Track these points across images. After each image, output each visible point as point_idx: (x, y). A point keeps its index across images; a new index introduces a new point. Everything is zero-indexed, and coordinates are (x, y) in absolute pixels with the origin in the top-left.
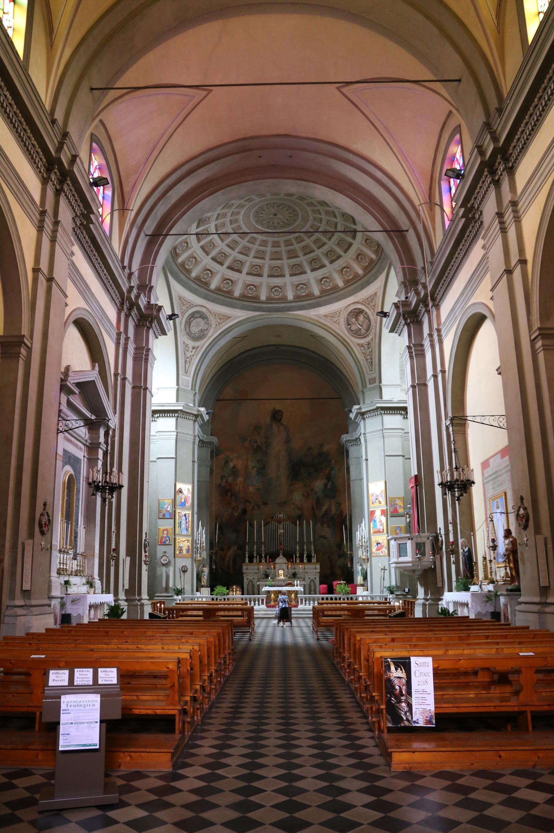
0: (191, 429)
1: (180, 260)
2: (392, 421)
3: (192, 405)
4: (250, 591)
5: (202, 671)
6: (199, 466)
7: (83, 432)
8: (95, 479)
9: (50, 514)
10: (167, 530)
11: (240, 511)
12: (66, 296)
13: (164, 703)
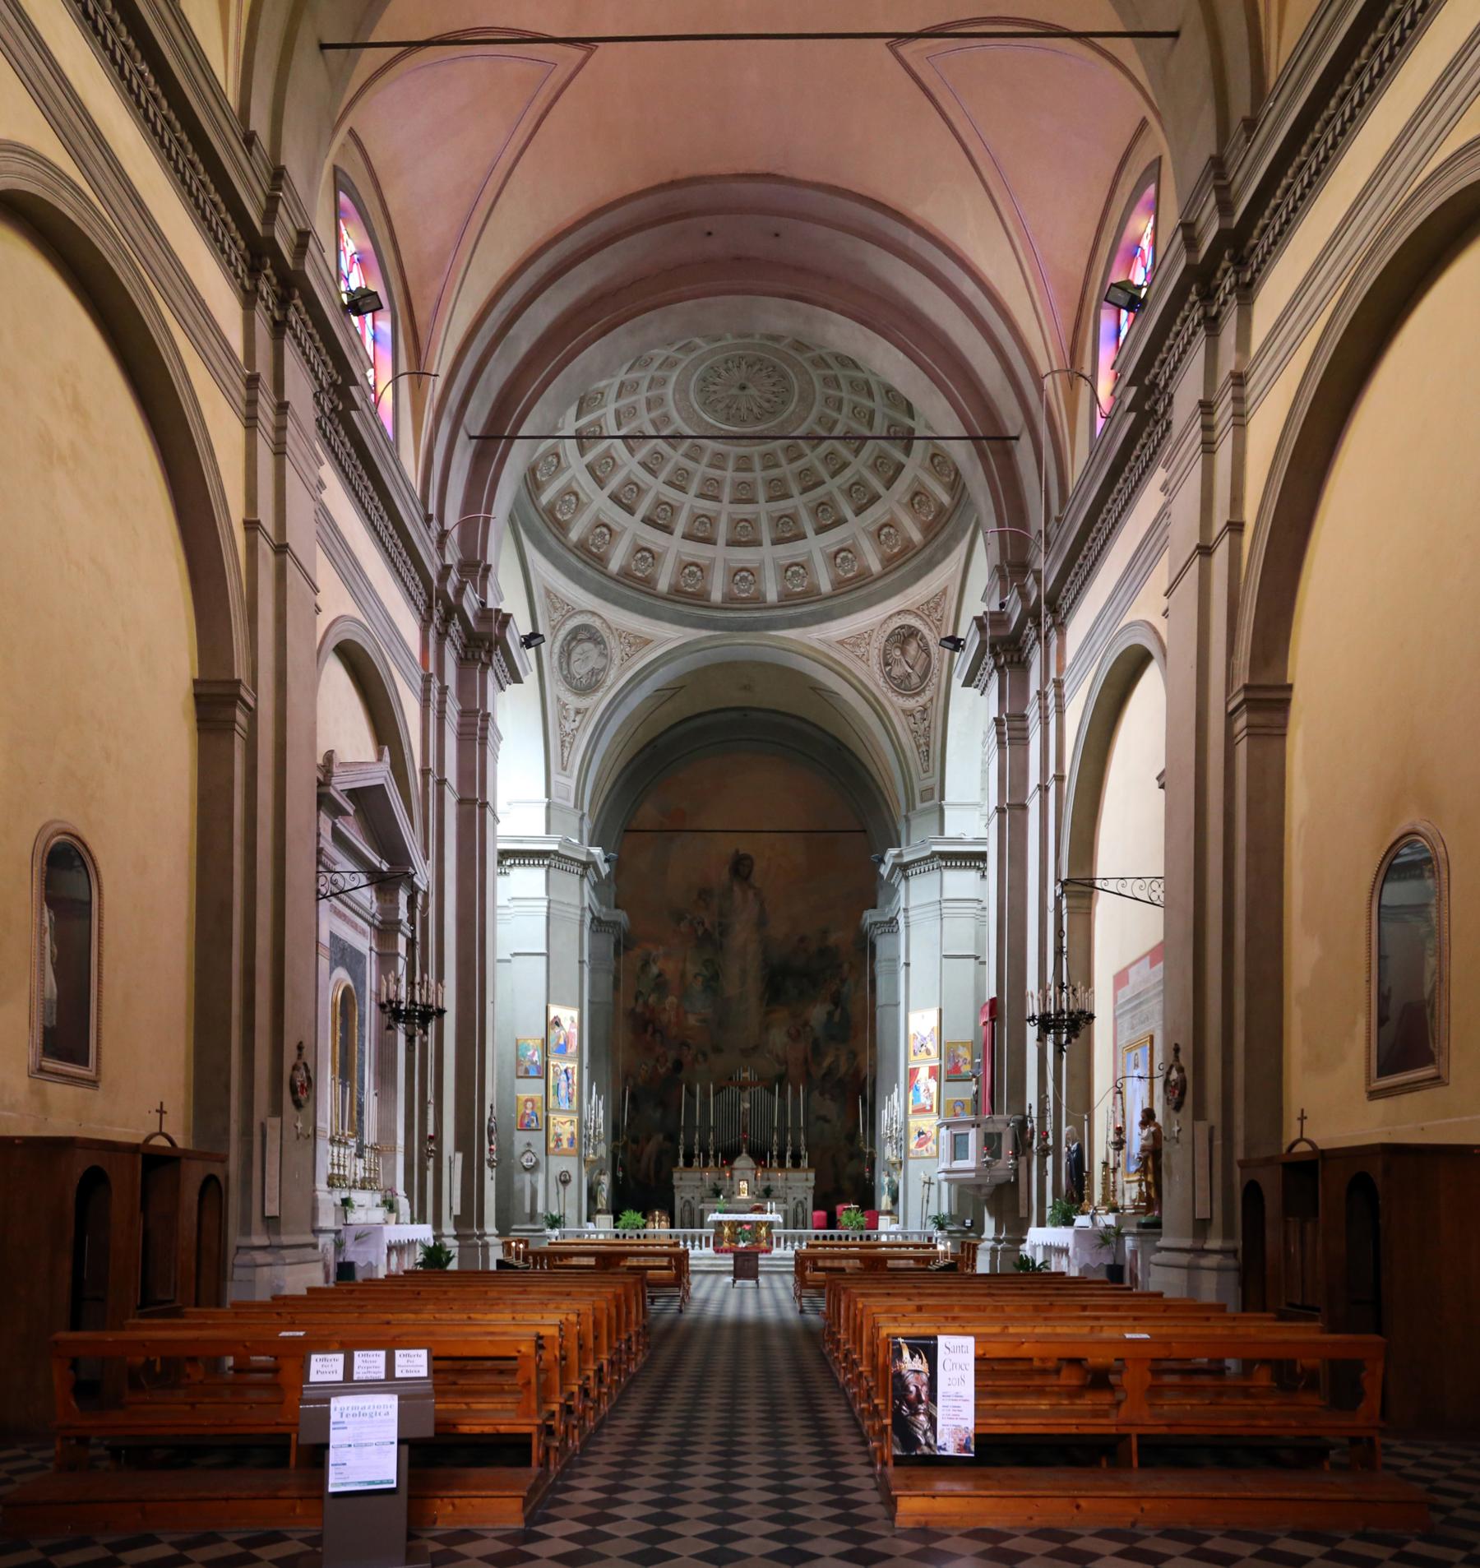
0: (577, 895)
1: (545, 499)
2: (960, 882)
3: (576, 841)
4: (686, 1220)
5: (583, 1361)
6: (592, 971)
7: (367, 897)
8: (392, 996)
9: (310, 1066)
10: (532, 1101)
11: (669, 1064)
12: (316, 590)
13: (513, 1415)
